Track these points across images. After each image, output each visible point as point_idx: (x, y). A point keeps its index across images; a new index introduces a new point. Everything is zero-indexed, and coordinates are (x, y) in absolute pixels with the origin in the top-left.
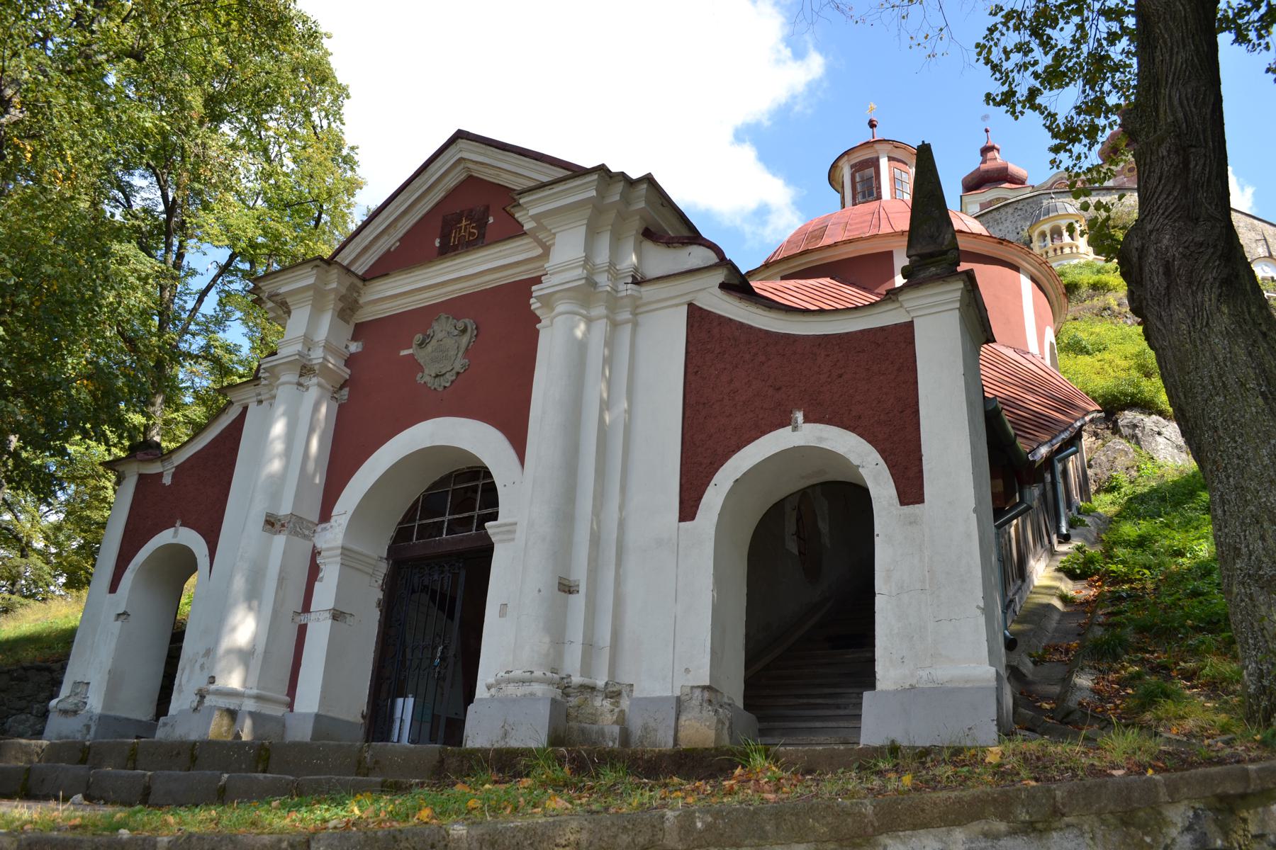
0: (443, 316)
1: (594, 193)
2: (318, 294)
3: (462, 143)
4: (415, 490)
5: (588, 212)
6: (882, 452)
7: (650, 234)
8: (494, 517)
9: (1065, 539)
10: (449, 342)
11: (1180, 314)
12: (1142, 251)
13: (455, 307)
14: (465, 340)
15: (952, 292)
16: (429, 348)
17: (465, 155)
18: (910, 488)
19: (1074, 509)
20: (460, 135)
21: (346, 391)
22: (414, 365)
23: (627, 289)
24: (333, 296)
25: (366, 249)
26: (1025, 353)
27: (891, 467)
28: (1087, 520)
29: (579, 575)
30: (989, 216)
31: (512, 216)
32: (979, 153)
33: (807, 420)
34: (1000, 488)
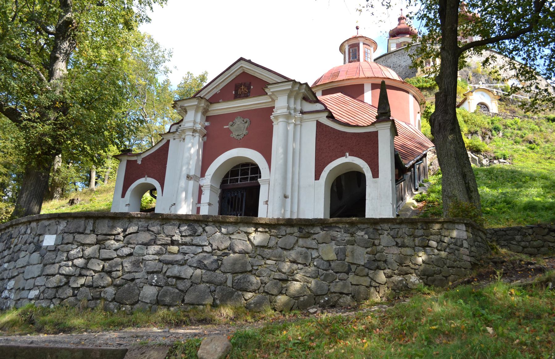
0: (239, 117)
1: (290, 87)
2: (197, 108)
3: (242, 62)
4: (229, 169)
5: (288, 92)
6: (369, 165)
7: (305, 99)
8: (260, 177)
9: (417, 190)
10: (242, 125)
11: (441, 136)
12: (434, 120)
13: (244, 114)
14: (246, 125)
15: (388, 125)
16: (235, 127)
18: (375, 174)
19: (421, 181)
20: (241, 59)
21: (205, 138)
22: (229, 131)
23: (299, 115)
24: (202, 108)
25: (209, 92)
26: (408, 124)
27: (371, 169)
28: (425, 185)
29: (289, 193)
30: (400, 51)
31: (264, 90)
32: (397, 20)
33: (349, 155)
34: (397, 173)
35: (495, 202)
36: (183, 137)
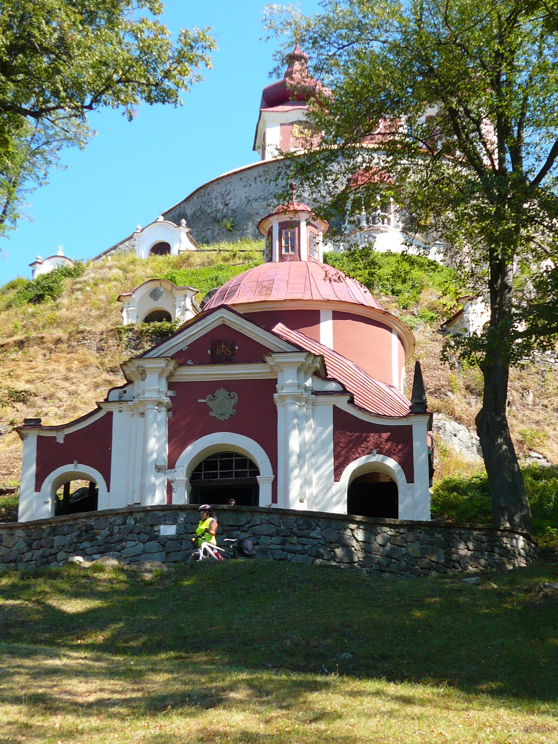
0: (222, 389)
3: (223, 310)
7: (316, 374)
13: (229, 385)
17: (224, 316)
18: (410, 479)
35: (206, 696)
36: (141, 410)
